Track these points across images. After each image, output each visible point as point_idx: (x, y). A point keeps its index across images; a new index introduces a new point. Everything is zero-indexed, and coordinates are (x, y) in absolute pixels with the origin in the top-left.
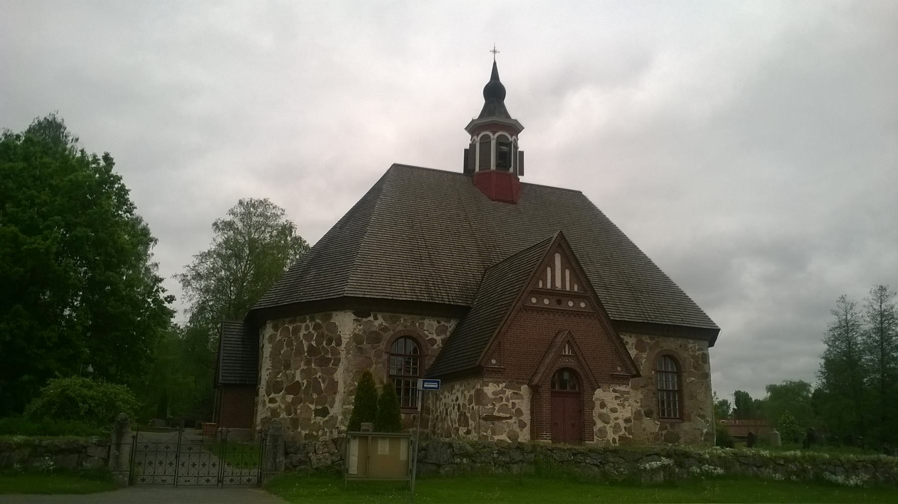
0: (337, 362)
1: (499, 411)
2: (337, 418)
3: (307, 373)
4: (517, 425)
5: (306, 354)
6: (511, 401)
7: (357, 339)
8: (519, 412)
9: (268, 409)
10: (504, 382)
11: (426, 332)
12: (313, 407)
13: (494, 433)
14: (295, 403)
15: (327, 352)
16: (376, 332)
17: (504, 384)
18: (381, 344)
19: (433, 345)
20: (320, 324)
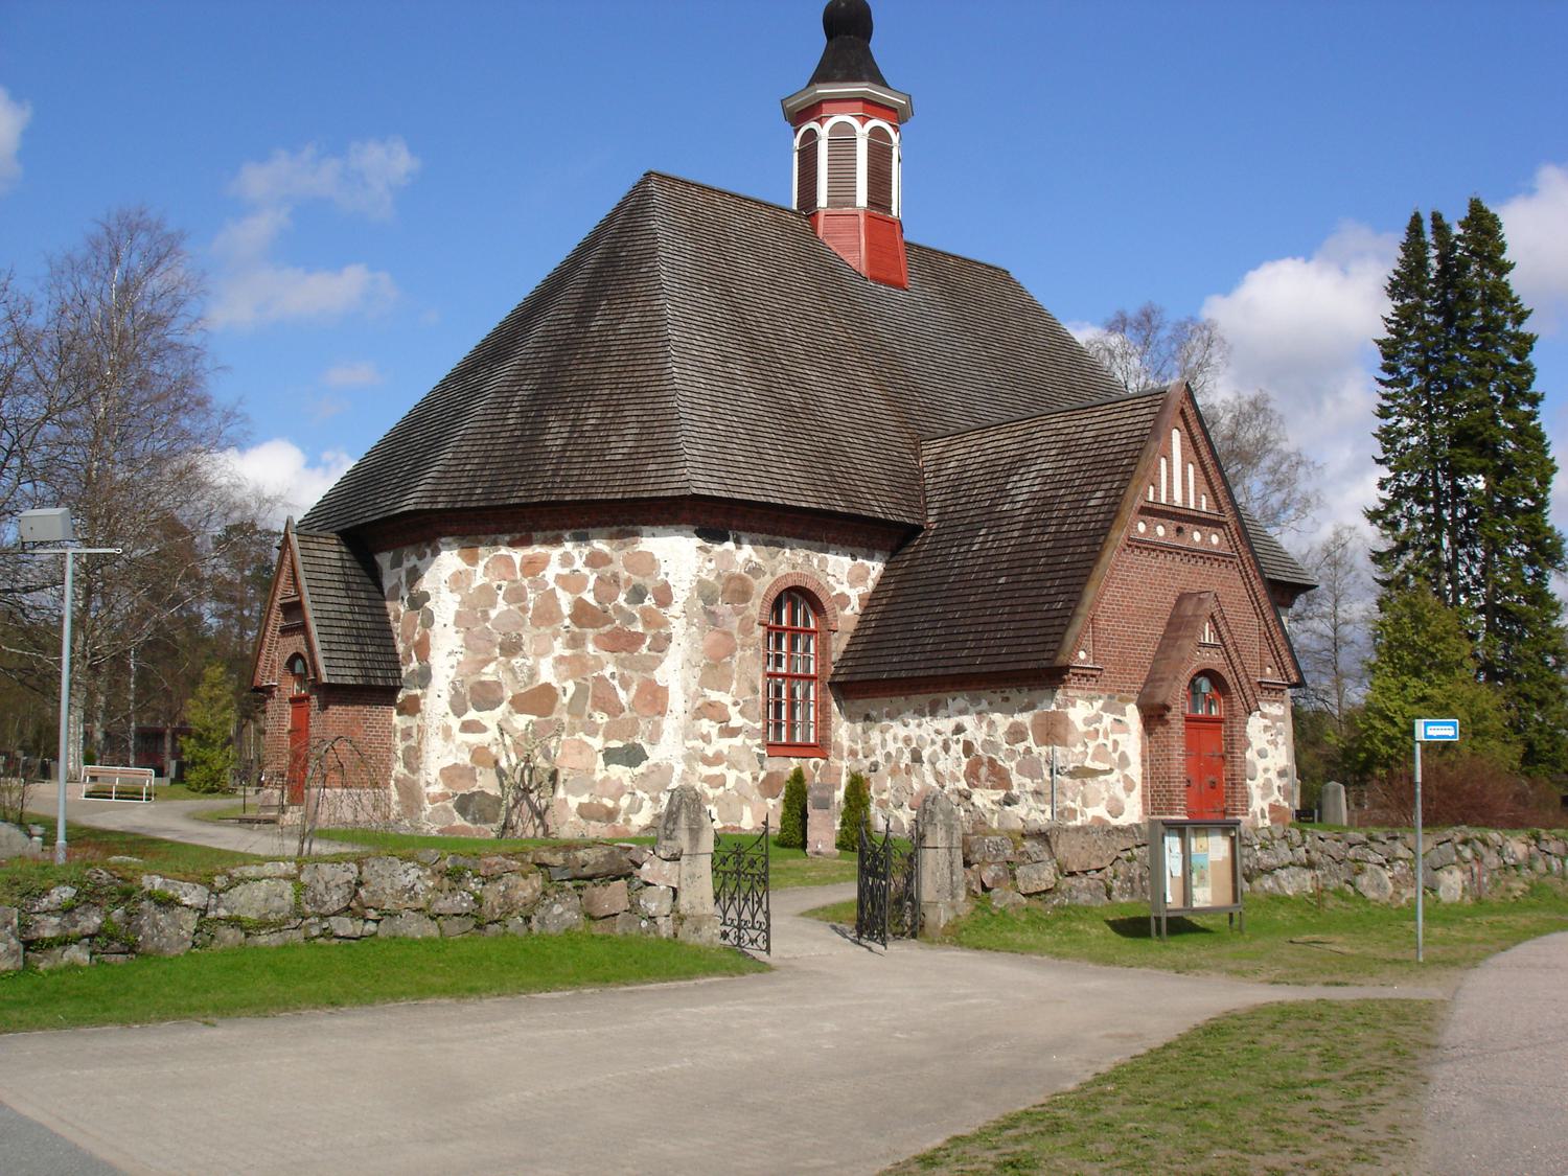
0: (662, 643)
1: (1095, 757)
2: (672, 768)
3: (575, 665)
4: (1122, 784)
5: (567, 622)
6: (1112, 737)
7: (706, 594)
8: (1124, 760)
9: (460, 746)
10: (1100, 698)
11: (830, 579)
12: (598, 743)
13: (1085, 804)
14: (537, 732)
15: (632, 619)
16: (740, 578)
17: (1101, 702)
18: (749, 604)
19: (843, 609)
20: (606, 555)
